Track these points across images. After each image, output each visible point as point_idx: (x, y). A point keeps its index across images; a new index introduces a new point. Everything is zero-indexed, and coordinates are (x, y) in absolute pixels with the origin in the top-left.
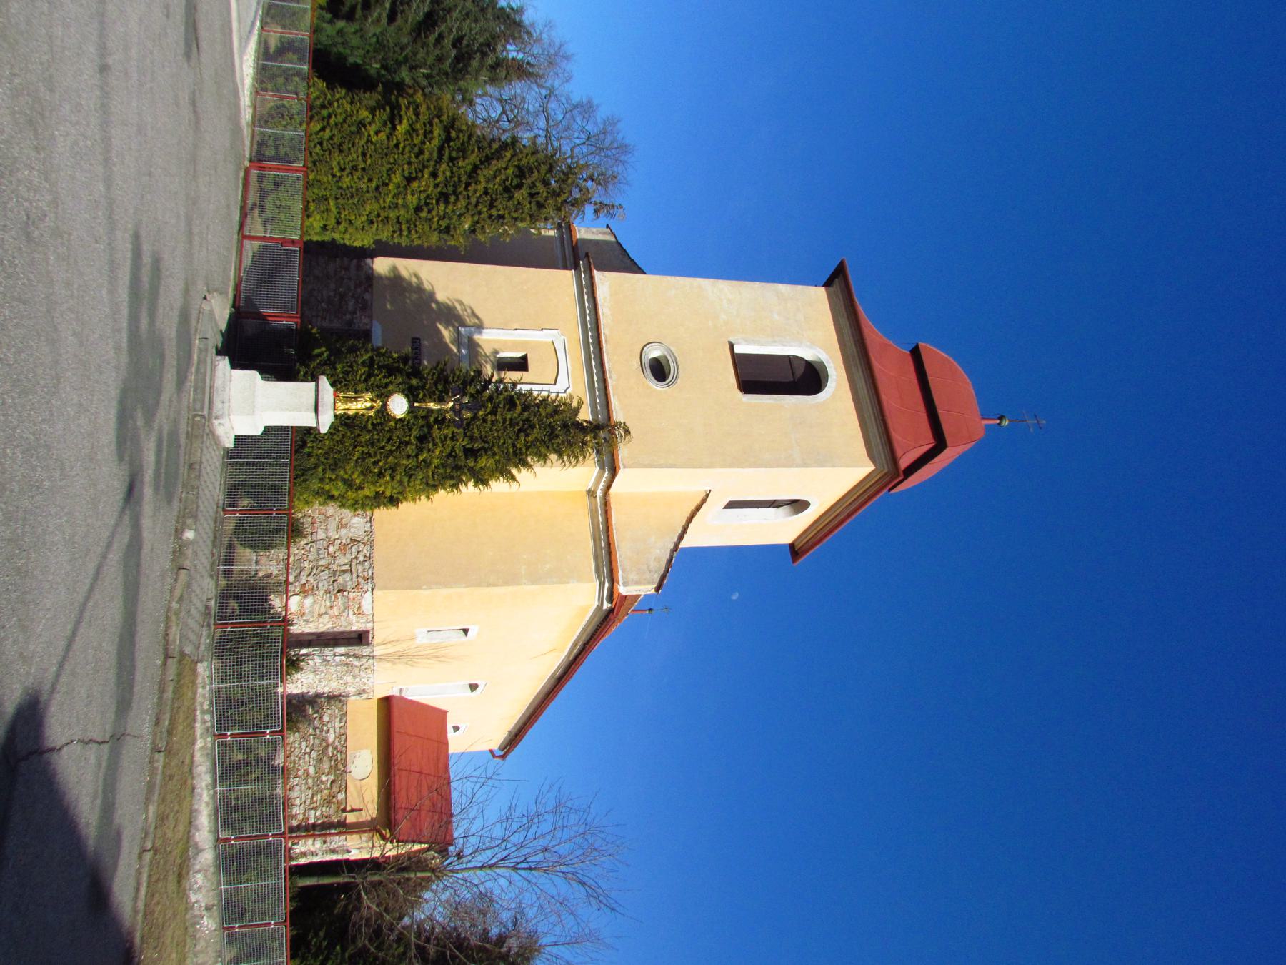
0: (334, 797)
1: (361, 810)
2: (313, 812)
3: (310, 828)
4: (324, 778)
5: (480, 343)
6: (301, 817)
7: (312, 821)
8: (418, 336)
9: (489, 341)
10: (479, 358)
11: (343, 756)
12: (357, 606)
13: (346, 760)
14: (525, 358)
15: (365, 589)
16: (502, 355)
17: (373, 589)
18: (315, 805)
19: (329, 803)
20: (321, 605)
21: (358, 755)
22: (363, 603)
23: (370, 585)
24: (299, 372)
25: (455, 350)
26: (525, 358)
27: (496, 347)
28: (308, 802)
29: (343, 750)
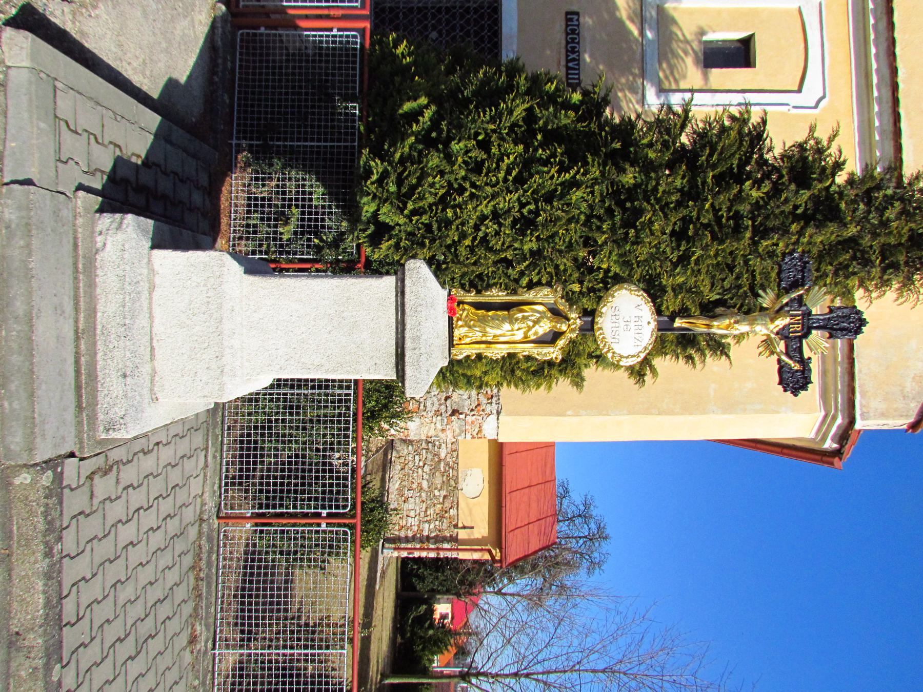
0: (446, 512)
1: (472, 528)
2: (427, 525)
3: (424, 539)
4: (437, 493)
5: (676, 15)
6: (416, 528)
7: (425, 533)
8: (575, 8)
9: (691, 12)
10: (674, 45)
11: (455, 473)
12: (477, 430)
13: (457, 476)
14: (747, 44)
15: (488, 411)
16: (710, 37)
17: (498, 413)
18: (428, 518)
19: (442, 517)
20: (430, 428)
21: (469, 473)
22: (485, 427)
23: (494, 406)
24: (368, 173)
25: (636, 33)
26: (747, 44)
27: (703, 23)
28: (422, 514)
29: (455, 466)
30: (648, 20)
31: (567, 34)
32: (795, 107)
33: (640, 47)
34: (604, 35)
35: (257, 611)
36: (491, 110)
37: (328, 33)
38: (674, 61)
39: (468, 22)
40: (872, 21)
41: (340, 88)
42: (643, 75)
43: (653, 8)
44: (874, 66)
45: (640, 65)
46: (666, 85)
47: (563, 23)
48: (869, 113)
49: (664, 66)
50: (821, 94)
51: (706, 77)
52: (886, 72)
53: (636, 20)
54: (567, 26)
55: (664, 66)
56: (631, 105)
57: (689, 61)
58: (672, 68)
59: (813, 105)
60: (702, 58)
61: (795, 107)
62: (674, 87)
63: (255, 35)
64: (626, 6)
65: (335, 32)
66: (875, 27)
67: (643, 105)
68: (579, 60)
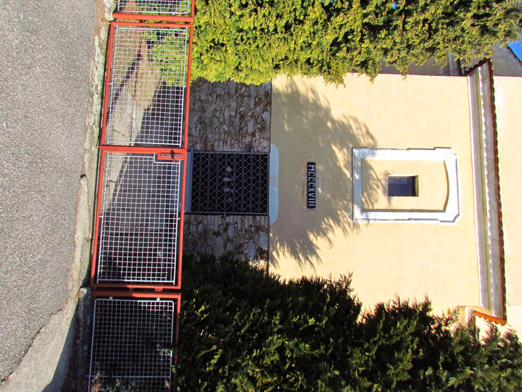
5: (373, 165)
8: (312, 160)
10: (371, 182)
14: (413, 180)
25: (349, 175)
26: (413, 180)
30: (356, 167)
31: (308, 176)
32: (442, 221)
33: (351, 185)
34: (330, 177)
35: (135, 260)
36: (257, 351)
37: (154, 301)
38: (371, 192)
39: (249, 181)
40: (486, 173)
41: (161, 339)
42: (353, 201)
43: (359, 160)
44: (488, 199)
45: (350, 195)
46: (366, 206)
47: (306, 169)
48: (484, 225)
49: (365, 194)
50: (457, 213)
51: (389, 201)
52: (495, 204)
53: (348, 167)
54: (308, 171)
55: (365, 194)
56: (345, 219)
57: (380, 191)
58: (369, 195)
59: (452, 219)
60: (387, 190)
61: (442, 221)
62: (371, 208)
63: (106, 302)
64: (343, 159)
65: (158, 300)
66: (488, 176)
67: (353, 220)
68: (315, 192)
